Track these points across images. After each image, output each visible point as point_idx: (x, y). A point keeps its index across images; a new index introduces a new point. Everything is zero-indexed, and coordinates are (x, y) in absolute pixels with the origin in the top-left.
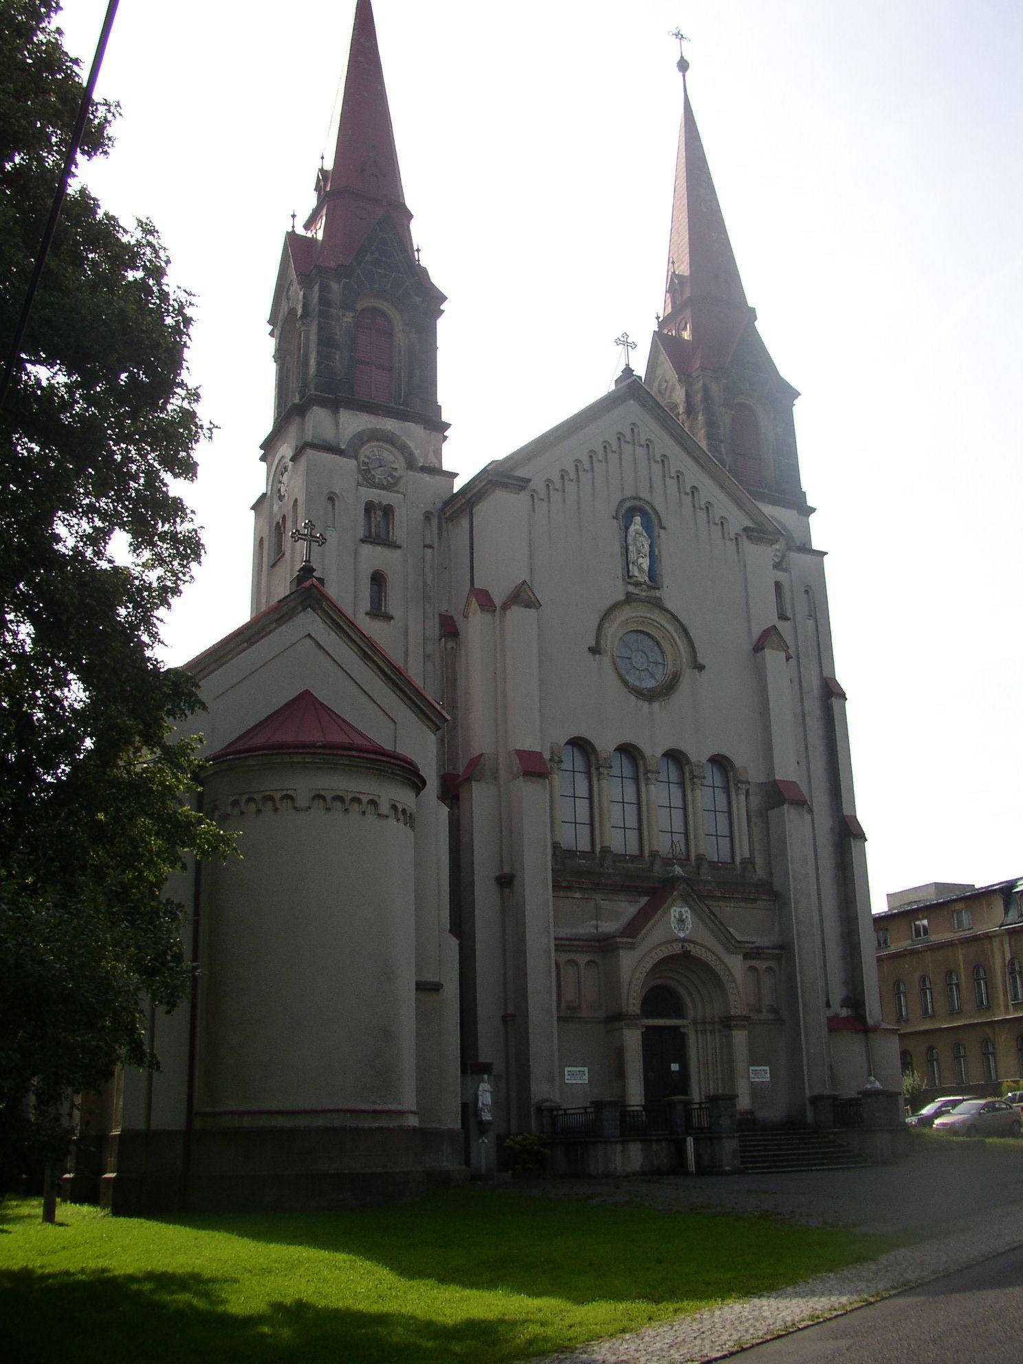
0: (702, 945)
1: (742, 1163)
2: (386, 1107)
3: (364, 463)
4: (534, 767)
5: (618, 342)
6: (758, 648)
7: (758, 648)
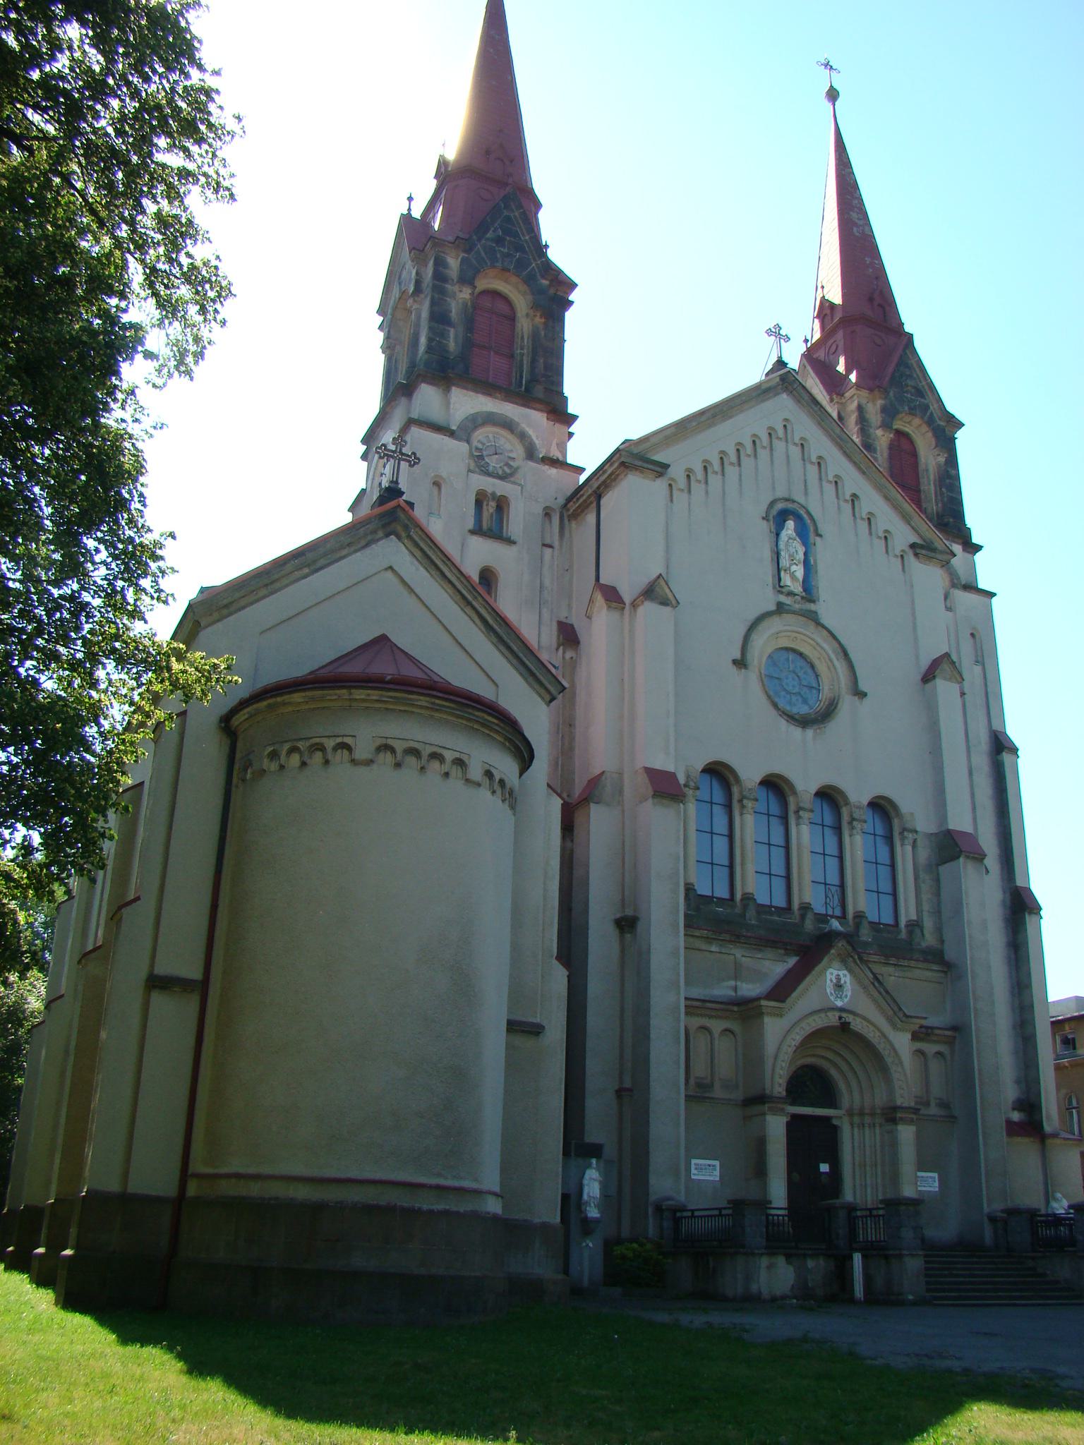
0: (864, 1018)
1: (928, 1290)
2: (456, 1183)
3: (477, 449)
4: (664, 787)
5: (769, 332)
6: (928, 676)
7: (928, 676)
